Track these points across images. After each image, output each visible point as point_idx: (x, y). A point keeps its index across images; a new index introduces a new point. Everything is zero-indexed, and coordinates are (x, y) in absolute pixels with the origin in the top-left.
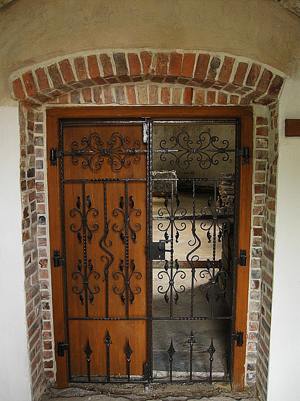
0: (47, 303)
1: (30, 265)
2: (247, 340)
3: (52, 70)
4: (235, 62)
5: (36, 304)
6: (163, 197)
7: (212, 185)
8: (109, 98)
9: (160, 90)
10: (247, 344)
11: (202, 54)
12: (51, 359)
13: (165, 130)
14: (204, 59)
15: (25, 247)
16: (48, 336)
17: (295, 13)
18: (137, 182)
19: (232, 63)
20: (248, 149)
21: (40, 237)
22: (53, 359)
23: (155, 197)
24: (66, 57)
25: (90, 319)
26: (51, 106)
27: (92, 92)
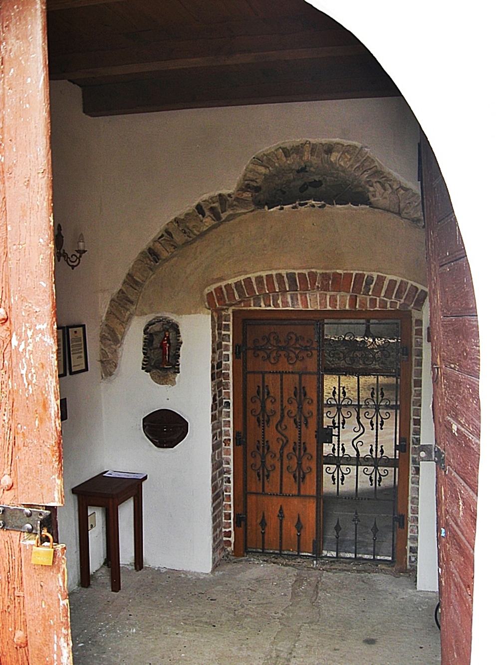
0: (229, 478)
1: (216, 441)
2: (409, 524)
3: (238, 285)
5: (219, 477)
6: (393, 376)
8: (285, 303)
9: (328, 297)
10: (409, 527)
12: (230, 529)
14: (360, 277)
15: (213, 426)
16: (228, 508)
18: (310, 373)
20: (407, 349)
21: (224, 419)
22: (232, 529)
24: (248, 276)
25: (266, 494)
26: (237, 308)
27: (271, 298)
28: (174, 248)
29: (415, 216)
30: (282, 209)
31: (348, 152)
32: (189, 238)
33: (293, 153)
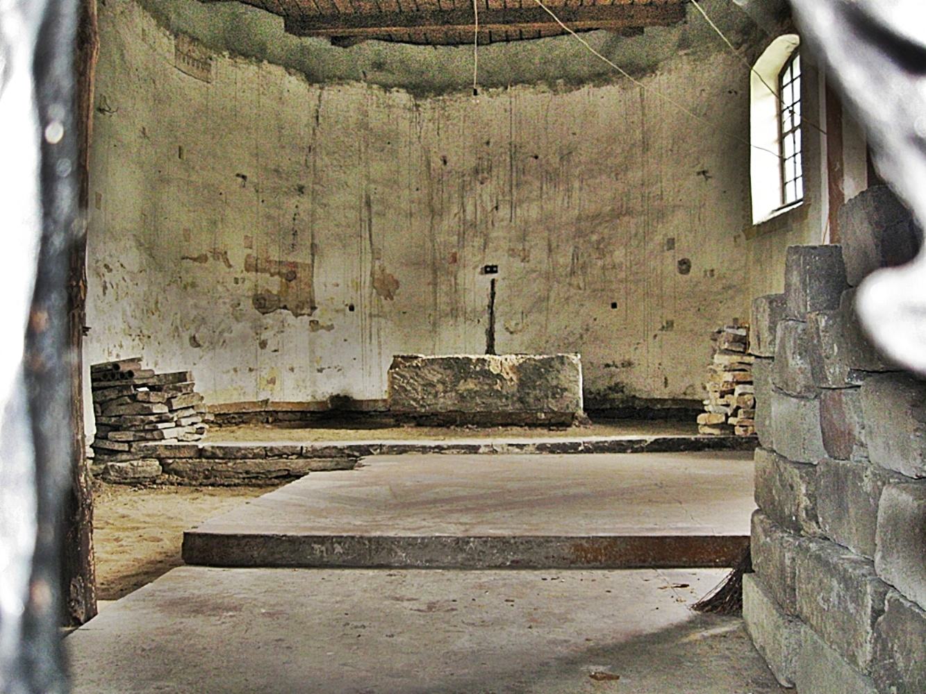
7: (685, 394)
13: (550, 250)
23: (521, 426)
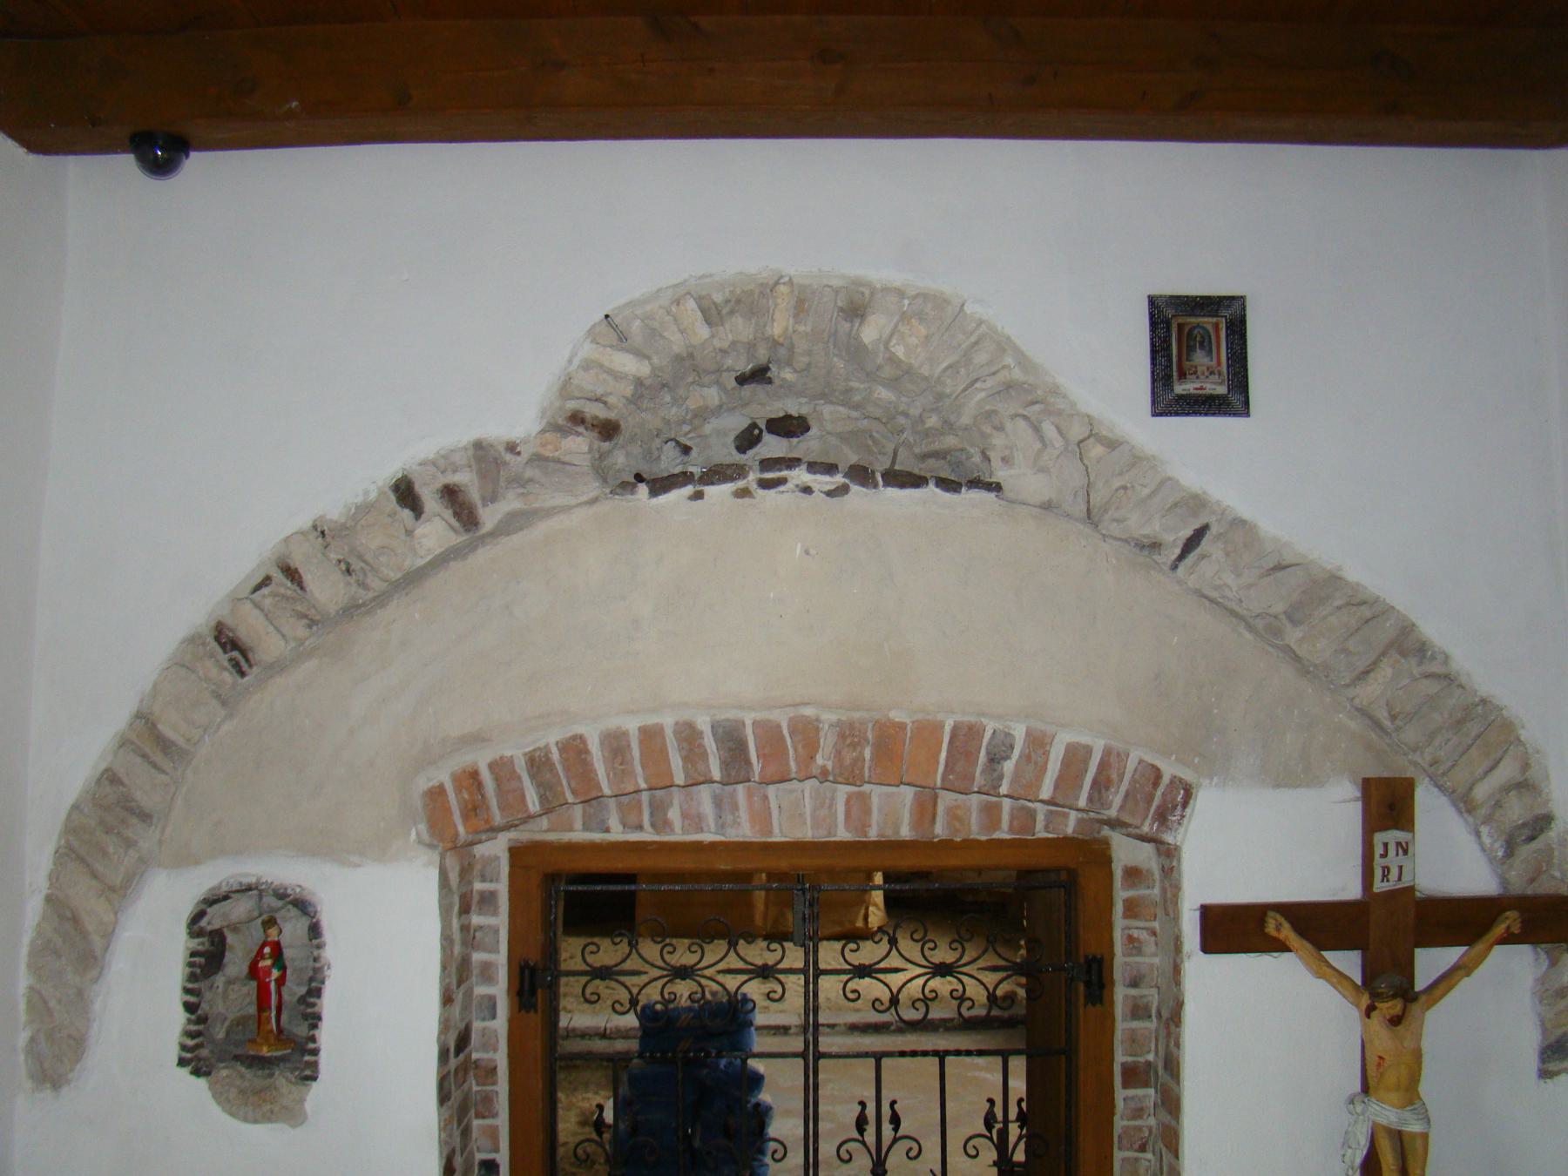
4: (1055, 741)
11: (962, 723)
17: (1221, 600)
19: (1048, 746)
28: (310, 627)
29: (1146, 531)
30: (698, 496)
31: (921, 317)
32: (361, 591)
33: (732, 312)
